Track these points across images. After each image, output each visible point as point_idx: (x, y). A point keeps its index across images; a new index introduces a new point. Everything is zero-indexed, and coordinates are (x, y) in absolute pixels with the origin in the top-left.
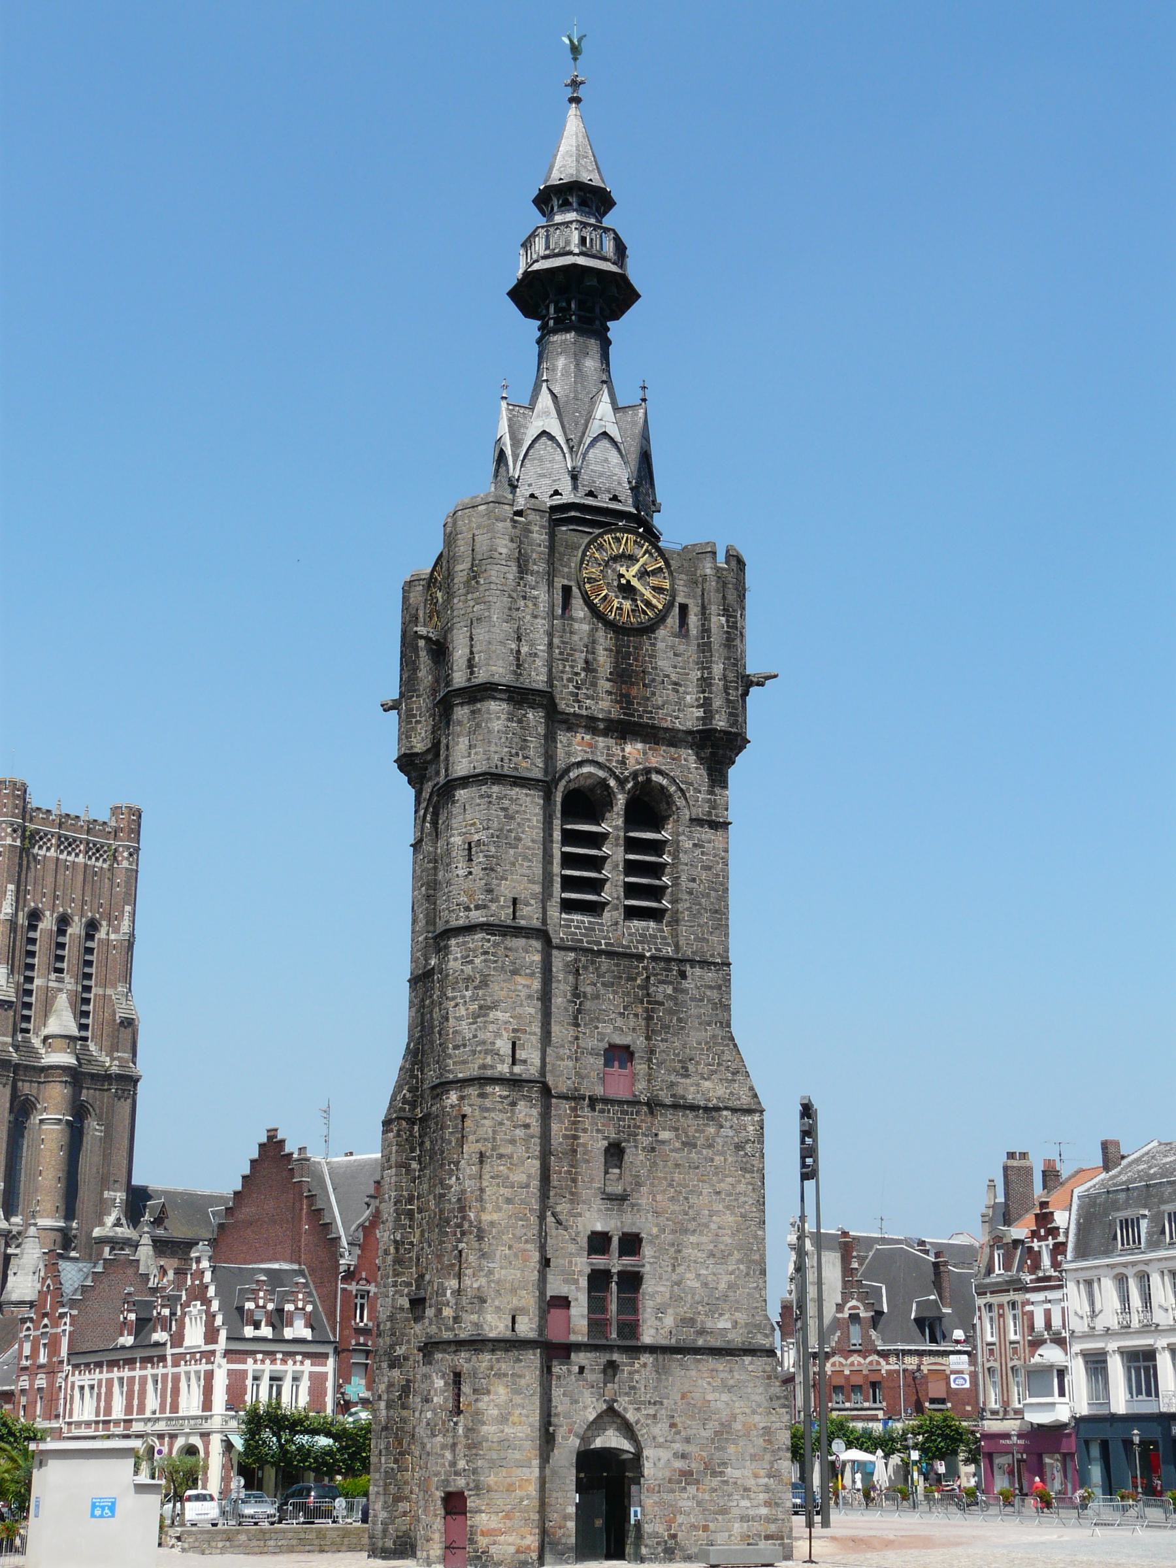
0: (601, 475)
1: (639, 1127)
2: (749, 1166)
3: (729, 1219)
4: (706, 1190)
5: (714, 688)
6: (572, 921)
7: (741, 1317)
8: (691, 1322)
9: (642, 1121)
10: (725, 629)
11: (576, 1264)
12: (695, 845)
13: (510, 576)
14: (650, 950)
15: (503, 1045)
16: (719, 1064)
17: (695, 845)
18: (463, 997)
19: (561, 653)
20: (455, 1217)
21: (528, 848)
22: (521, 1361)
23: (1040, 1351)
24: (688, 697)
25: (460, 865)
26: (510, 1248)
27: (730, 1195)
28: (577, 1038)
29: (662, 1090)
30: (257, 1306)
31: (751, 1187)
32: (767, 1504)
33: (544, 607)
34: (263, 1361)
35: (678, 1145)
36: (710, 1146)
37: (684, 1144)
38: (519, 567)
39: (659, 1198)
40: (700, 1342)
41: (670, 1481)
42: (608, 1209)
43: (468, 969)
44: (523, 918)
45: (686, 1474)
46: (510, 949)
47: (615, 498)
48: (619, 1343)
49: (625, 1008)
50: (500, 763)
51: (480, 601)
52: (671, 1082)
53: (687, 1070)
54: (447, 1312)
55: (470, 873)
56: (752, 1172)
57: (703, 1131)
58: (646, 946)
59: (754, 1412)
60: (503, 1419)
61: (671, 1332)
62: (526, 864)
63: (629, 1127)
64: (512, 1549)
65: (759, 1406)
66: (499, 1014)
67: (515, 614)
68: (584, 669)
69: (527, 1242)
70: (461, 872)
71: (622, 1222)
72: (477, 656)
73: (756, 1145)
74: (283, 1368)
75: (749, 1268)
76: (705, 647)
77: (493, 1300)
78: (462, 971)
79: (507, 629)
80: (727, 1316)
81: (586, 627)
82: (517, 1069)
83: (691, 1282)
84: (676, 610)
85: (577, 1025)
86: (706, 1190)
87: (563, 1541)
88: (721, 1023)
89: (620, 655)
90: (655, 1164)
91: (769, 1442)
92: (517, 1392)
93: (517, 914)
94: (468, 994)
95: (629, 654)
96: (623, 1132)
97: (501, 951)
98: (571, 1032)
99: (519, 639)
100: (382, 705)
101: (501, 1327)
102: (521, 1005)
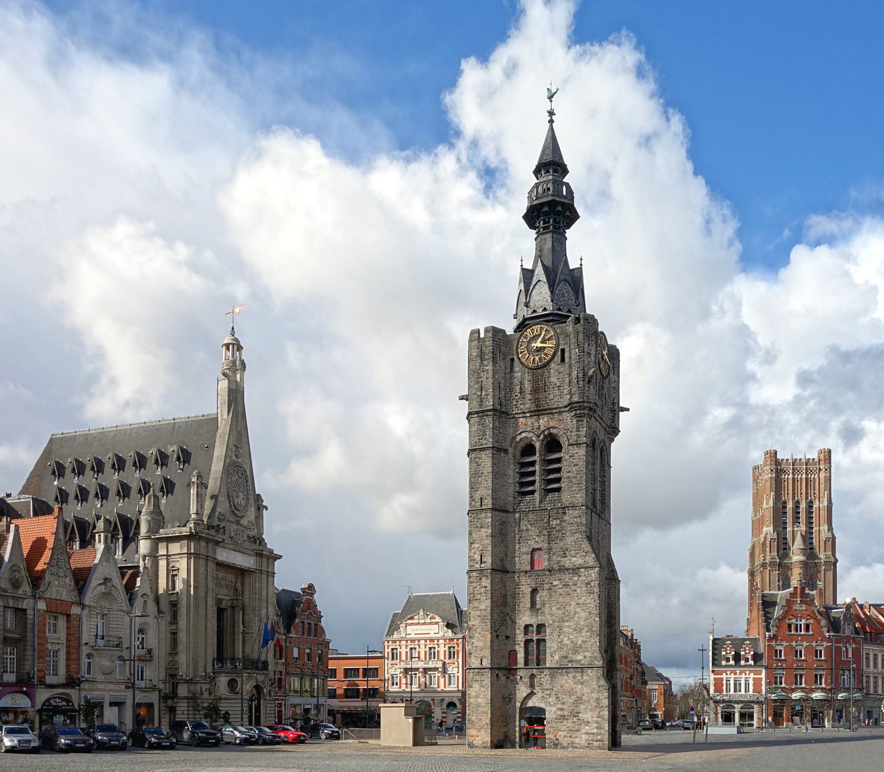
3: (583, 615)
7: (588, 654)
8: (566, 657)
9: (546, 578)
12: (570, 456)
15: (477, 557)
17: (570, 456)
29: (554, 564)
32: (597, 728)
34: (730, 674)
35: (561, 586)
37: (563, 585)
38: (481, 358)
39: (553, 609)
40: (570, 665)
41: (556, 719)
44: (484, 505)
45: (563, 717)
49: (539, 533)
53: (565, 554)
56: (594, 593)
59: (592, 692)
60: (477, 697)
64: (481, 742)
65: (594, 689)
66: (476, 545)
76: (570, 366)
80: (581, 654)
82: (482, 565)
83: (566, 641)
84: (559, 353)
89: (535, 381)
91: (599, 704)
92: (482, 686)
99: (482, 390)
101: (477, 663)
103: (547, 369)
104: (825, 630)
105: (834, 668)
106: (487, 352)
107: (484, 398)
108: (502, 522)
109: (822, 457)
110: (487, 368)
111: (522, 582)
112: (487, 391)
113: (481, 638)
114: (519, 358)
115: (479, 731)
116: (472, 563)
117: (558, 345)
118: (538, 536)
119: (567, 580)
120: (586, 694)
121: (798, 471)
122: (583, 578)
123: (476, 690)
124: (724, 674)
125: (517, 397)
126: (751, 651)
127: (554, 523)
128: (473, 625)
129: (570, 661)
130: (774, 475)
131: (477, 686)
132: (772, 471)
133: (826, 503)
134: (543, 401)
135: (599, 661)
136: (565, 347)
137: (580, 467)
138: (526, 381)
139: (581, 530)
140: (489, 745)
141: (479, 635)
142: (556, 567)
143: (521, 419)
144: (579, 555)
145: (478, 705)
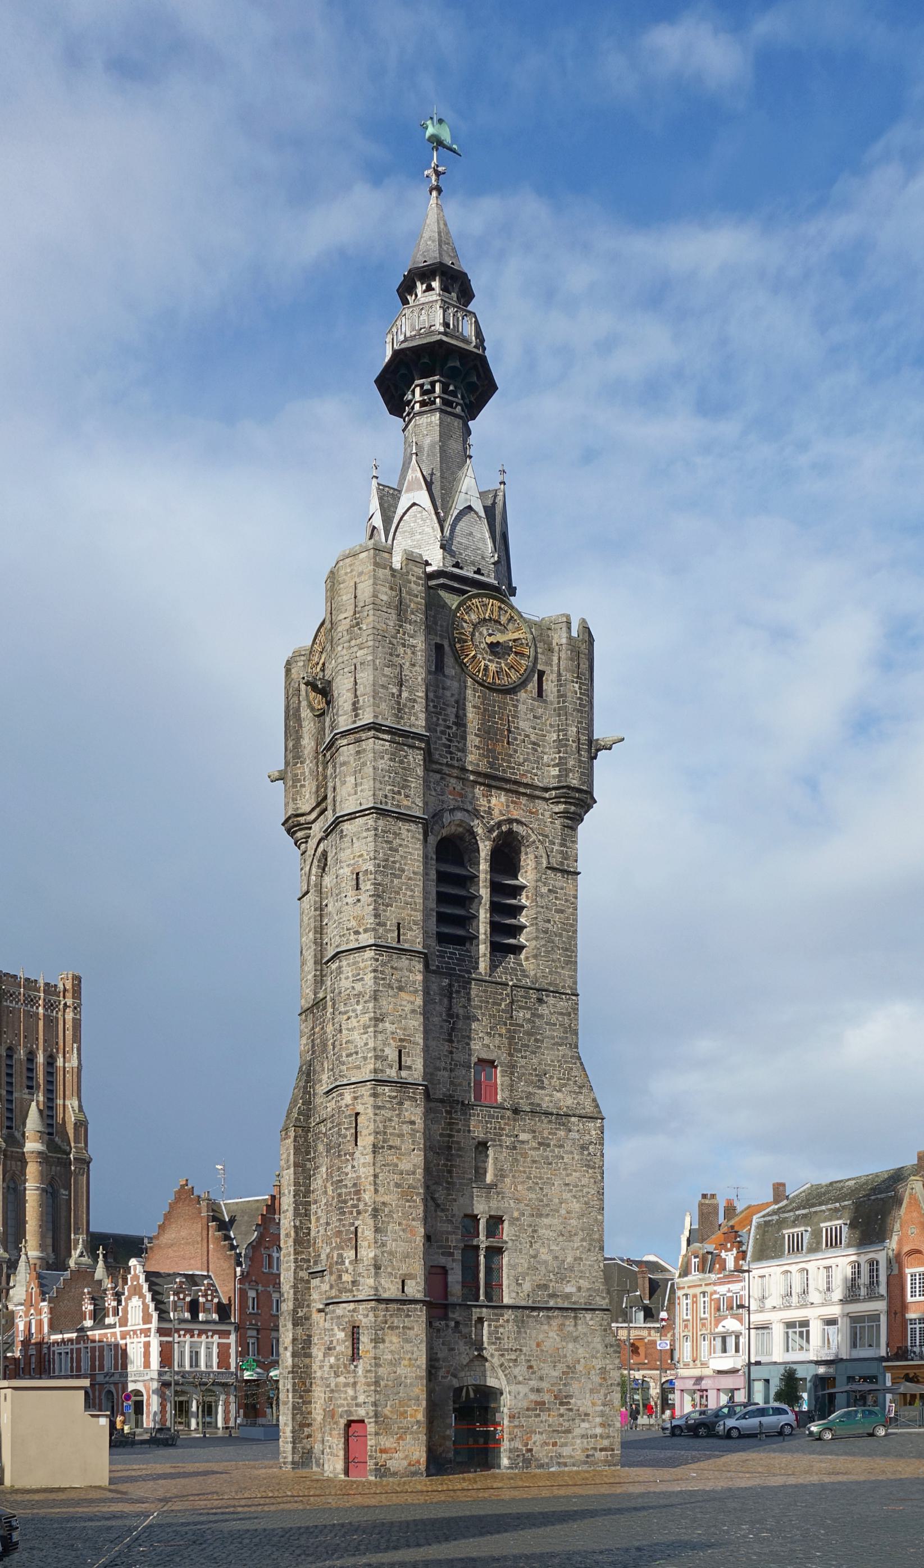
0: (466, 548)
1: (503, 1129)
6: (446, 952)
7: (584, 1284)
8: (545, 1287)
9: (505, 1124)
10: (578, 695)
11: (452, 1241)
13: (391, 623)
14: (512, 980)
15: (391, 1053)
17: (550, 890)
18: (354, 1011)
19: (435, 707)
20: (351, 1199)
22: (410, 1316)
23: (723, 1323)
24: (545, 757)
25: (349, 894)
26: (400, 1224)
27: (576, 1186)
29: (522, 1098)
30: (207, 1300)
31: (592, 1180)
32: (602, 1425)
33: (422, 656)
34: (184, 1335)
36: (561, 1146)
37: (540, 1144)
39: (520, 1187)
40: (551, 1304)
41: (528, 1409)
43: (358, 986)
44: (406, 941)
46: (396, 969)
47: (478, 572)
48: (487, 1303)
50: (384, 800)
51: (363, 646)
52: (529, 1092)
54: (346, 1277)
55: (359, 900)
56: (595, 1168)
57: (556, 1134)
58: (508, 977)
59: (593, 1357)
61: (528, 1295)
62: (409, 893)
63: (495, 1128)
64: (405, 1463)
68: (455, 723)
70: (350, 900)
71: (489, 1207)
72: (361, 699)
73: (597, 1146)
77: (386, 1268)
78: (353, 988)
79: (389, 674)
80: (573, 1282)
82: (404, 1073)
83: (544, 1255)
85: (451, 1041)
87: (444, 1455)
92: (407, 1341)
94: (359, 1008)
96: (490, 1133)
98: (446, 1046)
100: (269, 777)
102: (406, 1018)
105: (626, 1325)
107: (405, 705)
109: (69, 986)
113: (401, 1233)
115: (401, 1438)
116: (379, 1065)
119: (546, 1134)
120: (582, 1360)
121: (32, 1000)
122: (574, 1135)
123: (393, 1348)
126: (215, 1297)
127: (521, 1015)
128: (384, 1203)
129: (553, 1296)
131: (395, 1339)
133: (75, 1063)
135: (604, 1298)
137: (568, 918)
138: (469, 707)
139: (569, 1041)
140: (423, 1467)
143: (453, 781)
144: (568, 1088)
145: (399, 1382)
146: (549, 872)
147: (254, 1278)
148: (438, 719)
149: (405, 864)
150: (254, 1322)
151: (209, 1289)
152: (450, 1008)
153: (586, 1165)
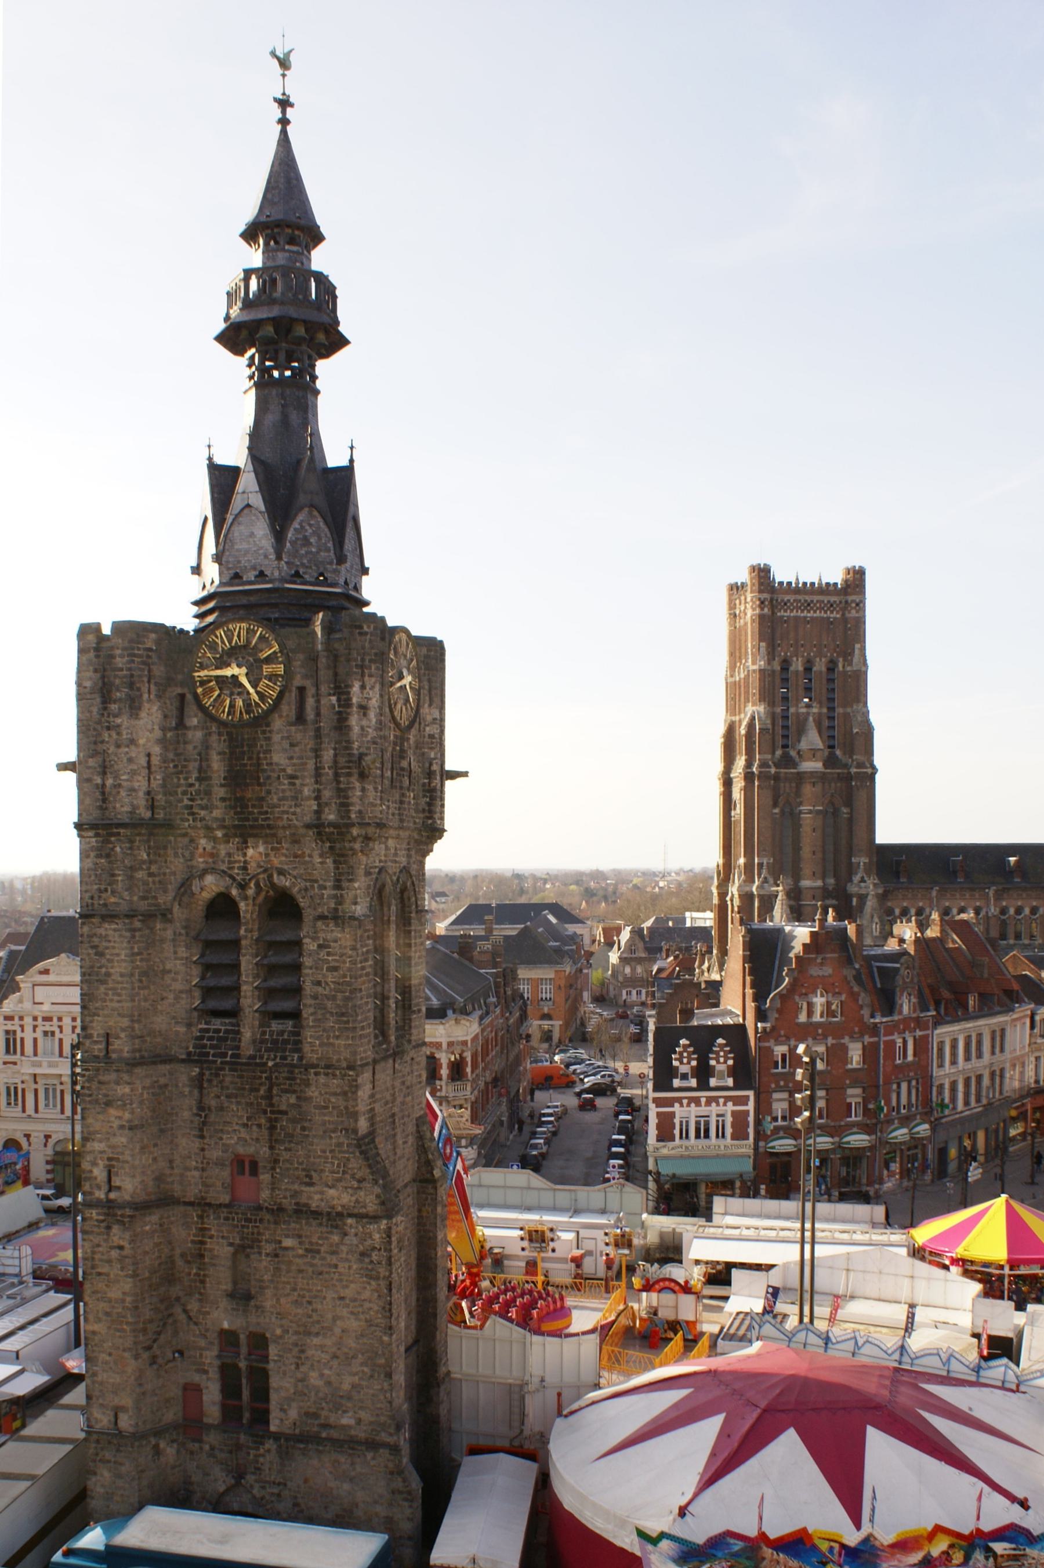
0: (247, 552)
2: (374, 1273)
3: (354, 1324)
4: (330, 1295)
5: (324, 779)
8: (315, 1416)
13: (95, 710)
16: (344, 1172)
17: (320, 946)
21: (118, 983)
28: (203, 1150)
29: (285, 1198)
34: (725, 1104)
35: (300, 1252)
36: (333, 1253)
37: (306, 1250)
38: (103, 696)
39: (283, 1300)
40: (324, 1435)
42: (233, 1309)
49: (248, 1119)
53: (310, 1177)
56: (377, 1278)
57: (327, 1238)
59: (376, 1502)
62: (116, 998)
63: (253, 1234)
67: (100, 747)
69: (124, 1350)
71: (247, 1322)
74: (708, 1108)
75: (373, 1370)
76: (318, 734)
80: (350, 1414)
81: (199, 734)
82: (113, 1195)
84: (294, 693)
86: (330, 1295)
88: (347, 1130)
90: (277, 1269)
92: (119, 1476)
93: (110, 1047)
95: (243, 753)
97: (95, 1085)
98: (197, 1144)
99: (104, 773)
103: (264, 732)
104: (866, 1012)
106: (117, 681)
107: (110, 793)
108: (160, 1087)
110: (119, 721)
111: (209, 1229)
112: (116, 777)
114: (196, 696)
117: (288, 674)
118: (245, 1125)
124: (677, 1105)
125: (192, 789)
126: (730, 1058)
130: (766, 610)
131: (106, 1474)
132: (762, 603)
134: (253, 806)
136: (308, 683)
137: (345, 976)
141: (108, 1358)
142: (288, 1203)
144: (343, 1184)
146: (319, 924)
147: (782, 1033)
148: (179, 779)
149: (112, 967)
150: (782, 1083)
151: (685, 1051)
152: (200, 1101)
153: (366, 1276)
